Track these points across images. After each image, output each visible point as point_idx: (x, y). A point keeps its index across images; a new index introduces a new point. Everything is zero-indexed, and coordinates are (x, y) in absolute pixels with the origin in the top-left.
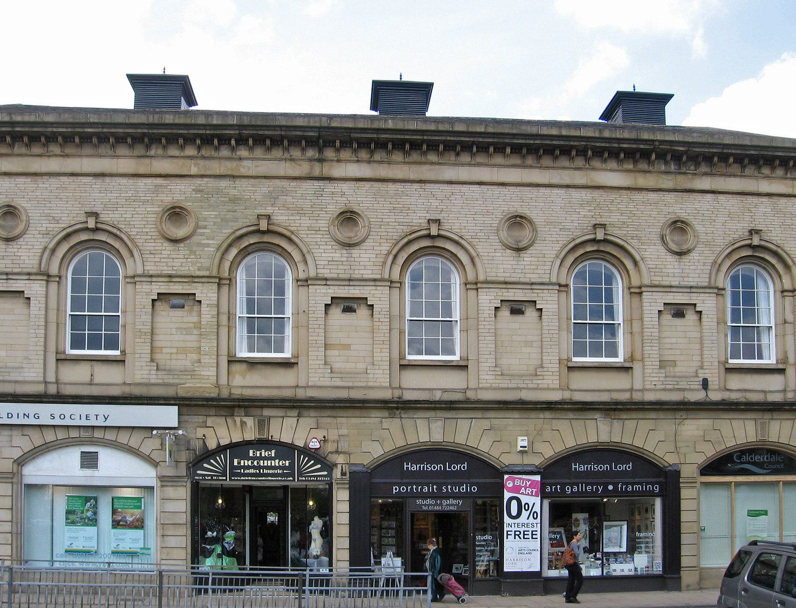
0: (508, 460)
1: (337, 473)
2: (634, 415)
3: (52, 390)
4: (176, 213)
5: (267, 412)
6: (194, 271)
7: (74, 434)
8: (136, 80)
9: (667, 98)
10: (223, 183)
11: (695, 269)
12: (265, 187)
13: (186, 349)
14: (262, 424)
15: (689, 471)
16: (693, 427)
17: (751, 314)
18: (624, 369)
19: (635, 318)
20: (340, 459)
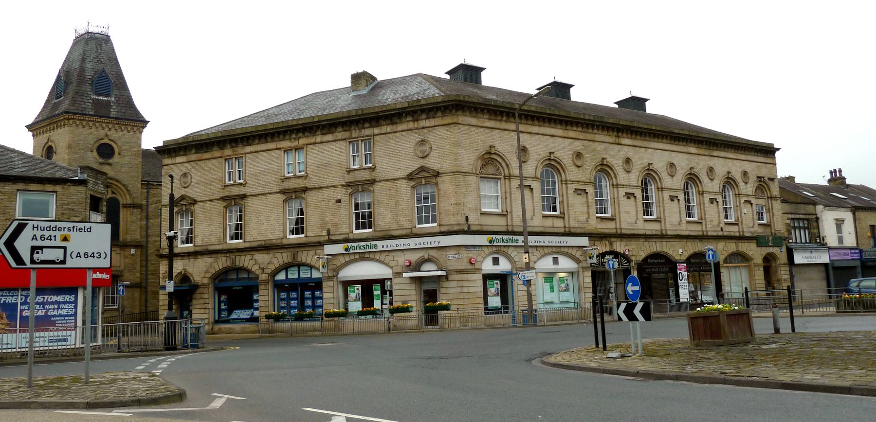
0: (677, 258)
1: (633, 264)
2: (306, 249)
3: (510, 229)
4: (579, 155)
5: (613, 239)
6: (584, 179)
7: (554, 249)
8: (448, 73)
9: (483, 69)
10: (591, 143)
11: (530, 169)
12: (604, 146)
13: (579, 211)
14: (611, 244)
15: (721, 262)
16: (721, 245)
17: (601, 195)
18: (611, 219)
19: (701, 204)
20: (633, 258)
